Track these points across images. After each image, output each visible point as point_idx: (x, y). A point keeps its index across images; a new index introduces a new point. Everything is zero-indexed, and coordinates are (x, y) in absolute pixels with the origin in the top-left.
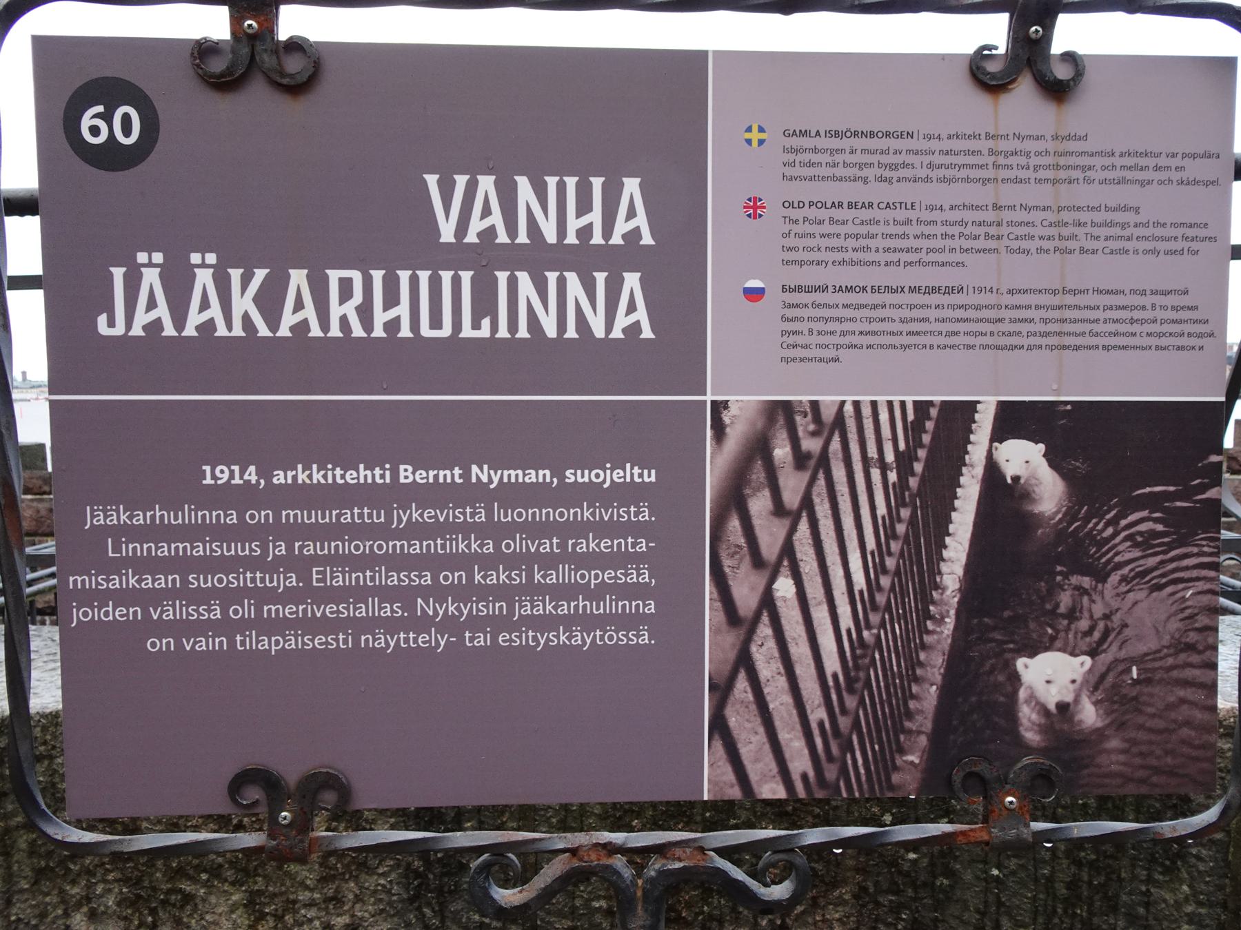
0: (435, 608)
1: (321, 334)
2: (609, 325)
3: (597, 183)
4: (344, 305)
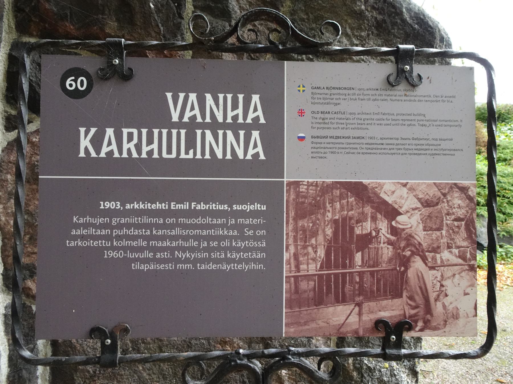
0: (182, 255)
1: (119, 156)
2: (245, 153)
3: (241, 97)
4: (129, 144)
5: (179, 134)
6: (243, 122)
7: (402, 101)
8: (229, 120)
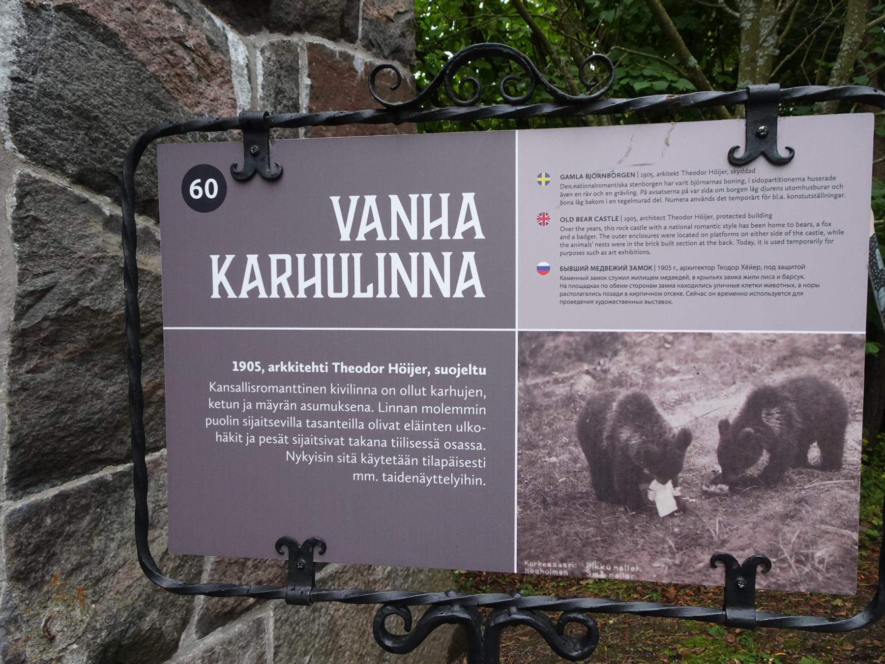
2: (453, 288)
3: (445, 197)
5: (351, 260)
6: (449, 238)
7: (687, 200)
8: (427, 236)
